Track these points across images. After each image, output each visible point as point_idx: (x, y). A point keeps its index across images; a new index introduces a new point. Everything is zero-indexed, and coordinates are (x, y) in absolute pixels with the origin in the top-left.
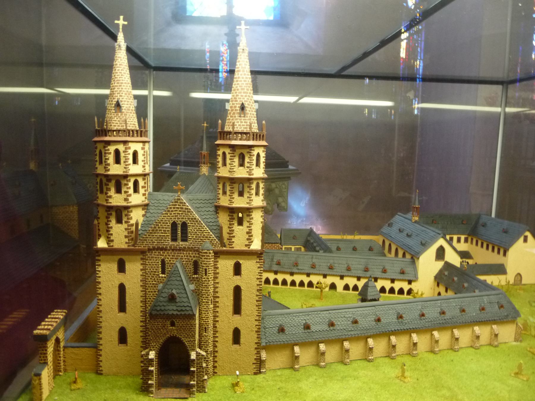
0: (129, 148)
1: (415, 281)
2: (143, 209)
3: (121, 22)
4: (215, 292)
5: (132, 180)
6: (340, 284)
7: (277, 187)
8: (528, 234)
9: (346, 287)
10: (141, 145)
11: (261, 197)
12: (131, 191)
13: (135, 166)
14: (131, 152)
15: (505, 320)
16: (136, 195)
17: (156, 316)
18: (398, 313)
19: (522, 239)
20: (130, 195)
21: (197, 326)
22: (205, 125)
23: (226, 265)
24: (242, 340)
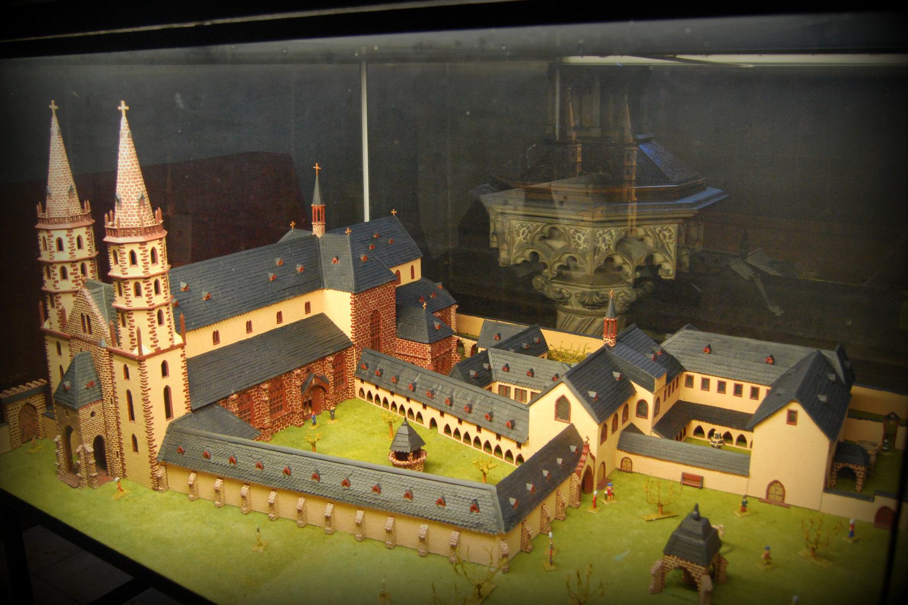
0: (52, 236)
1: (524, 444)
2: (74, 296)
3: (53, 107)
4: (114, 392)
5: (59, 267)
6: (441, 422)
7: (647, 235)
8: (795, 406)
9: (447, 429)
10: (66, 232)
11: (163, 294)
12: (58, 277)
13: (80, 251)
14: (54, 239)
15: (473, 530)
16: (64, 282)
17: (196, 410)
18: (317, 471)
19: (783, 415)
20: (57, 282)
21: (200, 432)
22: (317, 167)
23: (118, 365)
24: (139, 449)
